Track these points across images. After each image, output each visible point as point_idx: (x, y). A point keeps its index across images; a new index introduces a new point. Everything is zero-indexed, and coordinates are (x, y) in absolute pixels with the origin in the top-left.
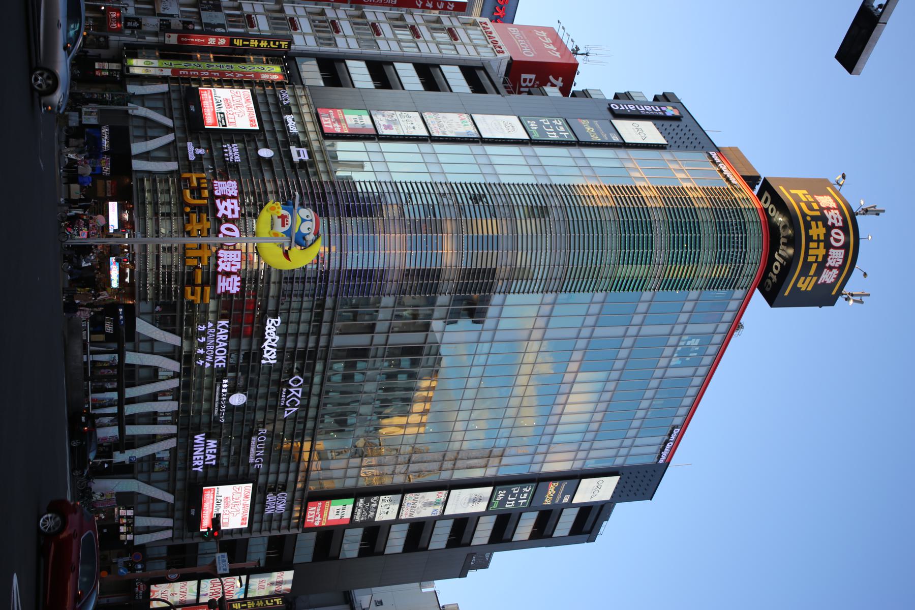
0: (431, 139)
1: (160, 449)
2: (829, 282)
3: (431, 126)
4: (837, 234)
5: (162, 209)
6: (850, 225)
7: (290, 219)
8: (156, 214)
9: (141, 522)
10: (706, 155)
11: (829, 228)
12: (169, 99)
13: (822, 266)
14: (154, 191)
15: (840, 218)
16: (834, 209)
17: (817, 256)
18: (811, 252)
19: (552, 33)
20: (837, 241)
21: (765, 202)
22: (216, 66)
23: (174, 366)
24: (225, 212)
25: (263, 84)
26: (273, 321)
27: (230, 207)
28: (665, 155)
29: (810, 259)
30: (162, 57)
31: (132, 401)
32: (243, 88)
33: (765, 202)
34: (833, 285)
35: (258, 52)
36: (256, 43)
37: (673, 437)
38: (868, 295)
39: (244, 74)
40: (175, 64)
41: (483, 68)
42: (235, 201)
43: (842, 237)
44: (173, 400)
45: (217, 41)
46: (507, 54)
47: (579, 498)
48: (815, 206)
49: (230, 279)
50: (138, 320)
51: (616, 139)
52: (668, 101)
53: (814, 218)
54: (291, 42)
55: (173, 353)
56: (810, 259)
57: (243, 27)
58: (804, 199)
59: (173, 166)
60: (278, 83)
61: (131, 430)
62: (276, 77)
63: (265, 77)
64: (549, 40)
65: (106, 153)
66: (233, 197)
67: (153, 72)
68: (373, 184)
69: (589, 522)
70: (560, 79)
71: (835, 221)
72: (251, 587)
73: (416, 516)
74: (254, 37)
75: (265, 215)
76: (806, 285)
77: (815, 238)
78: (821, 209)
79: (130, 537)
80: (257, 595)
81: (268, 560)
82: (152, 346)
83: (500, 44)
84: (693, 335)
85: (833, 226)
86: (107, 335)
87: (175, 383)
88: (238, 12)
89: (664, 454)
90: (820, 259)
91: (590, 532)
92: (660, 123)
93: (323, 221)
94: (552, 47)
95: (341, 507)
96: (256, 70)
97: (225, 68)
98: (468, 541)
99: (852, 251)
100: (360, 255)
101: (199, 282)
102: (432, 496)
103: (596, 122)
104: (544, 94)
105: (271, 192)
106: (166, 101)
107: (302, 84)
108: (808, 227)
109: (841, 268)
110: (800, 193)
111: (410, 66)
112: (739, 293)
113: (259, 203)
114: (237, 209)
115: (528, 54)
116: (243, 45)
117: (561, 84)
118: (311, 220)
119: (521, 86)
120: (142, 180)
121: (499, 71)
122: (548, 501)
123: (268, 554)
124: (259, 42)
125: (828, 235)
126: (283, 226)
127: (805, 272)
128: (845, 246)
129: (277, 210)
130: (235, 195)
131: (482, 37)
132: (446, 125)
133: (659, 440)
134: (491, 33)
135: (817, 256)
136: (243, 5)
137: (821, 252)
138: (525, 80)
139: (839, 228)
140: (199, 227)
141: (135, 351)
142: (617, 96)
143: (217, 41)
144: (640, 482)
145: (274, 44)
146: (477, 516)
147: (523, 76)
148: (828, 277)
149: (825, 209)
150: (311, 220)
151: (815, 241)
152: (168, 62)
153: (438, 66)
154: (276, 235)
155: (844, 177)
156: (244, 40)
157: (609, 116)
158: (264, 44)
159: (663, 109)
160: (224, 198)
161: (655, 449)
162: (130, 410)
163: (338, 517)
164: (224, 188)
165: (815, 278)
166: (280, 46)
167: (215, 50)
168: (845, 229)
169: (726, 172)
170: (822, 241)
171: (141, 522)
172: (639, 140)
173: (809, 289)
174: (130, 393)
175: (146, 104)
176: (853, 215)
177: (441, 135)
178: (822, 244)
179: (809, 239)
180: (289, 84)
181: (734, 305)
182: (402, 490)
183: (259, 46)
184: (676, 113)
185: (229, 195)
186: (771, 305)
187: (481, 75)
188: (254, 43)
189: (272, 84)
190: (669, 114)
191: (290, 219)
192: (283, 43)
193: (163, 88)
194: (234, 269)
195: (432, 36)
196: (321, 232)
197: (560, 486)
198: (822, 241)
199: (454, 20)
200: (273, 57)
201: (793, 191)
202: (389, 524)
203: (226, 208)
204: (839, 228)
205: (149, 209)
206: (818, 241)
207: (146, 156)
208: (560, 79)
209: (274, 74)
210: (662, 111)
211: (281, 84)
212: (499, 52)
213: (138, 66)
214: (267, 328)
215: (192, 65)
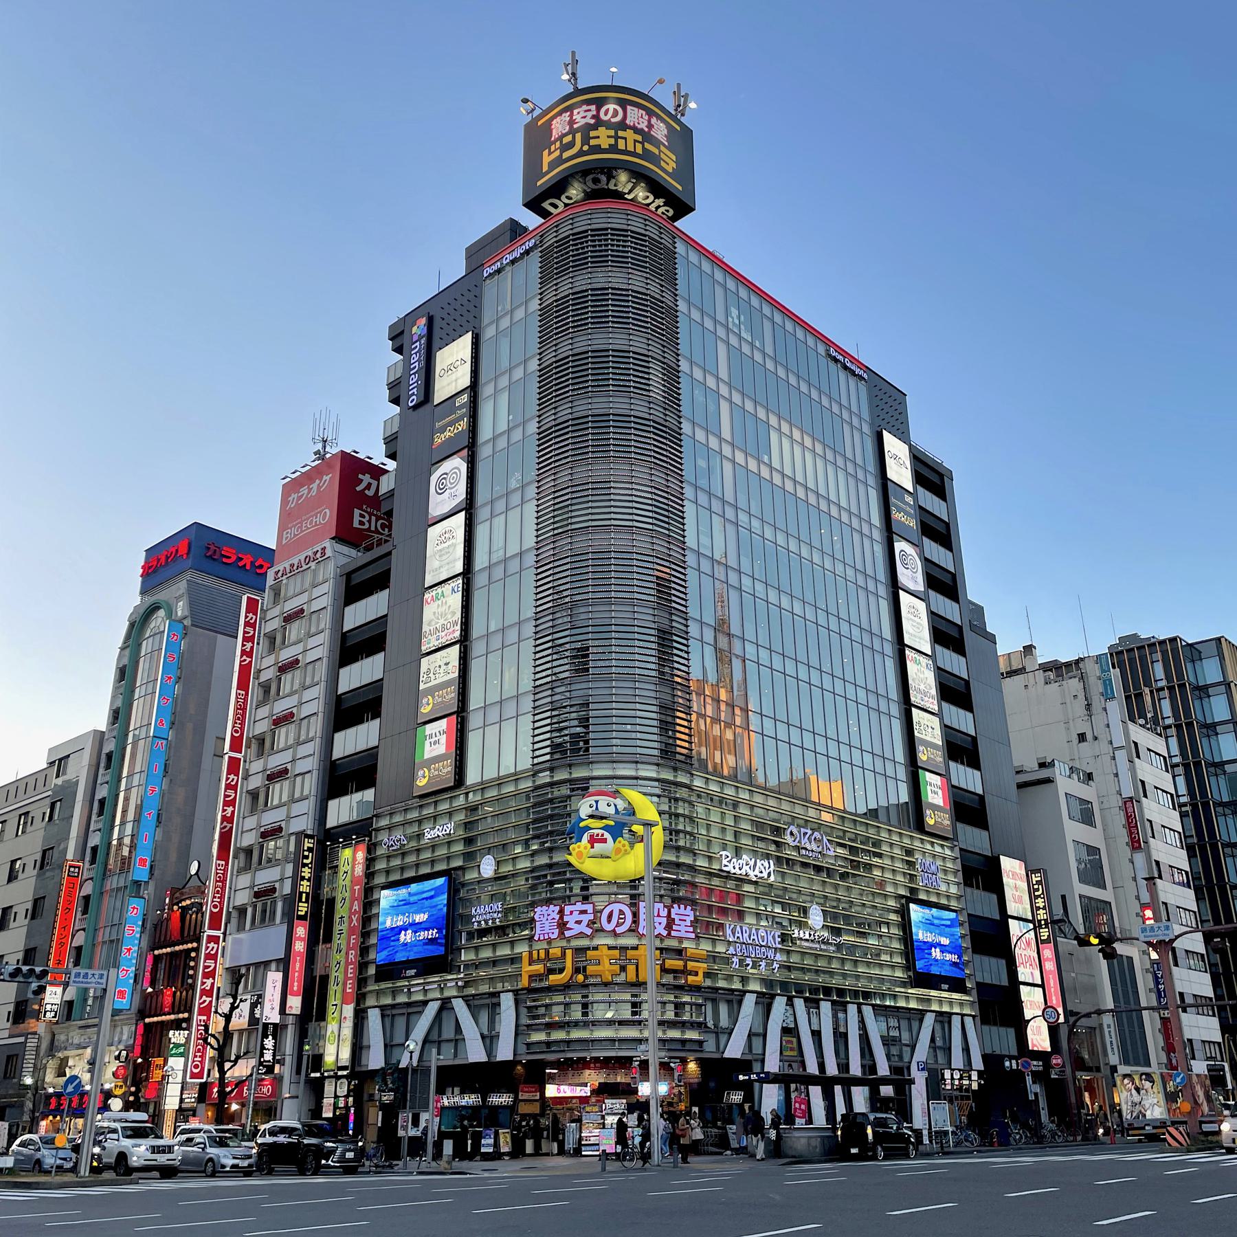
0: (464, 641)
1: (876, 1030)
2: (665, 132)
3: (444, 640)
4: (606, 113)
5: (577, 1014)
6: (595, 96)
7: (596, 832)
8: (586, 1025)
9: (958, 1060)
10: (488, 281)
11: (598, 123)
12: (393, 1006)
13: (646, 136)
14: (551, 1026)
15: (585, 107)
16: (571, 115)
17: (635, 141)
18: (631, 148)
19: (292, 487)
20: (616, 113)
21: (556, 207)
22: (339, 940)
23: (780, 1003)
24: (585, 923)
25: (370, 874)
26: (725, 862)
27: (576, 916)
28: (489, 333)
29: (639, 150)
30: (322, 1016)
31: (844, 1067)
32: (378, 901)
33: (556, 207)
34: (668, 126)
35: (317, 882)
36: (305, 883)
37: (840, 358)
38: (679, 85)
39: (353, 899)
40: (333, 999)
41: (349, 576)
42: (568, 909)
43: (611, 107)
44: (818, 1008)
45: (300, 939)
46: (327, 544)
47: (909, 485)
48: (569, 138)
49: (677, 918)
50: (726, 1055)
51: (465, 398)
52: (402, 332)
53: (586, 140)
54: (301, 835)
55: (765, 1002)
56: (639, 150)
57: (274, 903)
58: (557, 153)
59: (507, 1001)
60: (369, 851)
61: (856, 1069)
62: (361, 856)
63: (359, 870)
64: (304, 490)
65: (484, 1099)
66: (561, 912)
67: (347, 1032)
68: (537, 718)
69: (932, 477)
70: (360, 476)
71: (589, 114)
72: (1021, 914)
73: (933, 692)
74: (295, 886)
75: (589, 866)
76: (670, 162)
77: (612, 141)
78: (572, 132)
79: (974, 1076)
80: (1028, 906)
81: (986, 888)
82: (758, 1035)
83: (310, 553)
84: (727, 314)
85: (596, 117)
86: (745, 1100)
87: (799, 1003)
88: (250, 911)
89: (858, 371)
90: (639, 138)
91: (941, 476)
92: (436, 342)
93: (594, 786)
94: (314, 486)
95: (929, 788)
96: (347, 882)
97: (345, 927)
98: (956, 629)
99: (628, 96)
100: (618, 742)
101: (681, 963)
102: (911, 668)
103: (438, 425)
104: (391, 494)
105: (551, 858)
106: (394, 1012)
107: (371, 818)
108: (597, 149)
109: (650, 113)
110: (547, 159)
111: (344, 672)
112: (680, 248)
113: (568, 875)
114: (579, 906)
115: (327, 516)
116: (307, 901)
117: (367, 476)
118: (597, 802)
119: (369, 530)
120: (528, 1045)
121: (349, 556)
122: (912, 523)
123: (978, 888)
124: (303, 878)
125: (608, 125)
126: (605, 841)
127: (655, 160)
128: (623, 104)
129: (582, 849)
130: (558, 908)
131: (299, 577)
132: (442, 621)
133: (843, 375)
134: (292, 566)
135: (635, 141)
136: (238, 903)
137: (629, 134)
138: (361, 523)
139: (598, 110)
140: (606, 962)
141: (763, 1061)
142: (395, 401)
143: (300, 939)
144: (888, 408)
145: (307, 857)
146: (933, 615)
147: (356, 524)
148: (660, 131)
149: (571, 127)
150: (597, 802)
151: (616, 142)
152: (331, 1009)
153: (344, 636)
154: (618, 851)
155: (525, 101)
156: (300, 900)
157: (427, 407)
158: (306, 873)
159: (415, 338)
160: (562, 925)
161: (852, 381)
162: (832, 1070)
163: (940, 792)
164: (547, 924)
165: (662, 148)
166: (310, 850)
167: (312, 942)
168: (600, 103)
169: (516, 254)
170: (616, 133)
171: (958, 1060)
172: (467, 367)
173: (674, 158)
174: (812, 1068)
175: (401, 1041)
176: (578, 92)
177: (459, 627)
178: (621, 133)
179: (613, 149)
180: (370, 836)
181: (693, 257)
182: (907, 705)
183: (309, 880)
184: (423, 321)
185: (557, 917)
186: (691, 209)
187: (357, 579)
188: (305, 886)
189: (370, 861)
190: (420, 335)
191: (596, 832)
192: (307, 845)
193: (374, 1017)
194: (664, 913)
195: (295, 644)
196: (610, 789)
197: (896, 506)
198: (616, 133)
199: (269, 615)
200: (324, 861)
201: (545, 168)
202: (946, 728)
203: (579, 922)
204: (598, 110)
205: (576, 1034)
206: (617, 137)
207: (490, 1040)
208: (360, 476)
209: (354, 859)
210: (419, 340)
211: (371, 848)
212: (323, 554)
213: (336, 1052)
214: (733, 871)
215: (336, 974)
